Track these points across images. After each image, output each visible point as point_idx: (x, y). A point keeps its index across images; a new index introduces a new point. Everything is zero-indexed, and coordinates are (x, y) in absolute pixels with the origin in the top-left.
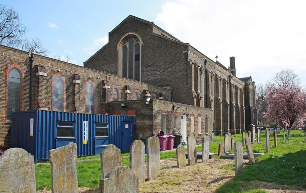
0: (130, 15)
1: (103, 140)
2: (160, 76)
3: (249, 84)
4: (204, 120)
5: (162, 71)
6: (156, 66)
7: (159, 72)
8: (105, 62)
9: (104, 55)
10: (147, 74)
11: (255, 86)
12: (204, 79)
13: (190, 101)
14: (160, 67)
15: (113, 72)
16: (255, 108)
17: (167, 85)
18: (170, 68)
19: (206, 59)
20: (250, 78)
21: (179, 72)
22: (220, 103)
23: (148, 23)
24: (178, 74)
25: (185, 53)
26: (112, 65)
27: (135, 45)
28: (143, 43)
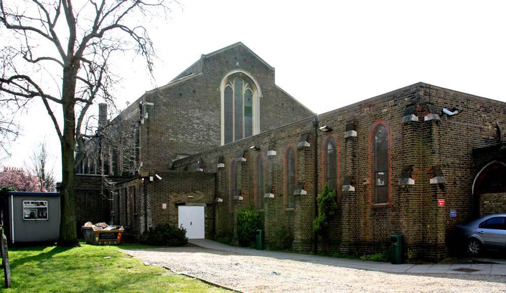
1: (38, 92)
8: (196, 103)
15: (212, 124)
26: (210, 112)
27: (246, 91)
28: (262, 94)
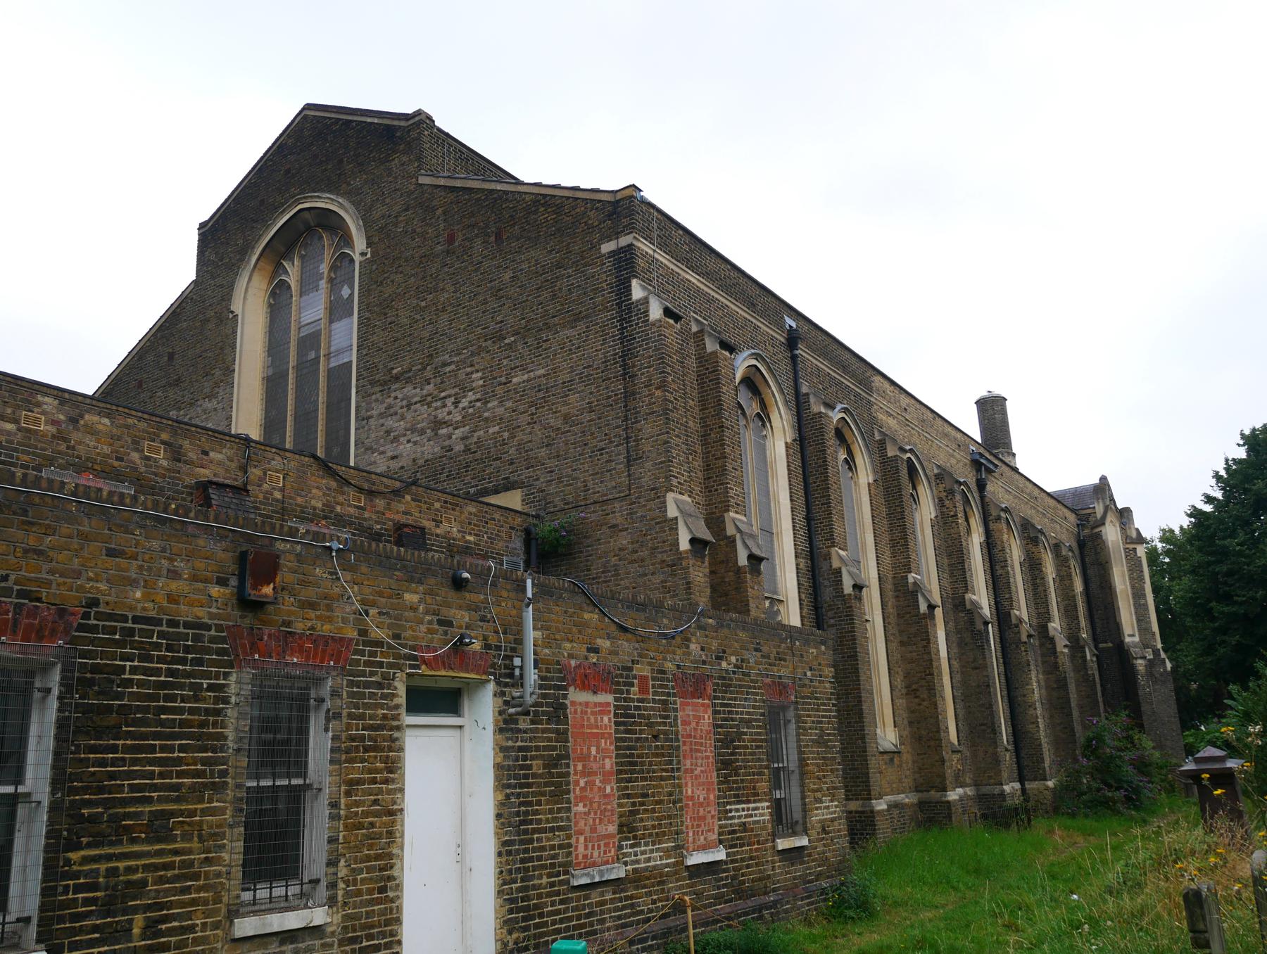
0: (309, 107)
2: (458, 433)
3: (1099, 516)
4: (748, 723)
5: (471, 396)
6: (436, 373)
7: (456, 403)
9: (171, 356)
10: (388, 432)
11: (1134, 535)
12: (787, 446)
13: (658, 579)
14: (461, 375)
16: (1156, 652)
17: (508, 486)
18: (524, 368)
19: (790, 322)
20: (1102, 489)
21: (581, 387)
22: (923, 608)
23: (396, 123)
24: (573, 398)
25: (613, 254)
28: (369, 245)
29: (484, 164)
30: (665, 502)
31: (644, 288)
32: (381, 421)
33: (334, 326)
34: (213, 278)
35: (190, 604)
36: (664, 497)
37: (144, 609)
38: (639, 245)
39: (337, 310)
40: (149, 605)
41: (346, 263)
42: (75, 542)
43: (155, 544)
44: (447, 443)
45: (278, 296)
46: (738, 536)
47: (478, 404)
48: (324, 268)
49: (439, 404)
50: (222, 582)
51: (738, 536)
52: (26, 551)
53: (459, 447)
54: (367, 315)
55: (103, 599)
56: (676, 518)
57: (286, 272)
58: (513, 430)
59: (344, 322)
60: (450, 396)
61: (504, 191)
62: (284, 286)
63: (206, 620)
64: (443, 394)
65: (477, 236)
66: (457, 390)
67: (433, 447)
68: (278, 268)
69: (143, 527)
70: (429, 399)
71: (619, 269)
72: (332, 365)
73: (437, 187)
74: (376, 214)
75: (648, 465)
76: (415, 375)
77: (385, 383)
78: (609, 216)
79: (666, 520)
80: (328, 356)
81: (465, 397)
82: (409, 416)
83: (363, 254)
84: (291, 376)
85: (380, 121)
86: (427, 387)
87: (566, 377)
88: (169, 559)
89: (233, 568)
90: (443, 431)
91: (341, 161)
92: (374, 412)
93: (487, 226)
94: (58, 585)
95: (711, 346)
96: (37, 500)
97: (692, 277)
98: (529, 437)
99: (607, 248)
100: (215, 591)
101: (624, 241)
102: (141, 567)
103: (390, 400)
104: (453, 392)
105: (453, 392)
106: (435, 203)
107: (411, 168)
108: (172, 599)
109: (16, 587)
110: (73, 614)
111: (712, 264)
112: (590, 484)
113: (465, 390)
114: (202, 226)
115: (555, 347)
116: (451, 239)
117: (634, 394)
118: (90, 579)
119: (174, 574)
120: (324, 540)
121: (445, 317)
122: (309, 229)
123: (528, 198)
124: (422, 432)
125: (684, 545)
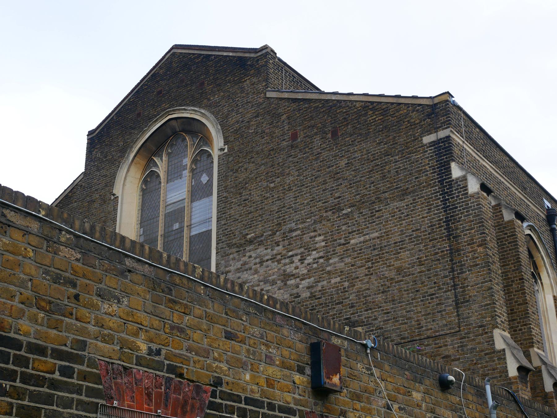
0: (176, 47)
2: (305, 283)
5: (315, 254)
6: (284, 237)
7: (302, 260)
18: (360, 232)
23: (247, 55)
24: (404, 255)
25: (433, 144)
28: (226, 143)
29: (308, 86)
30: (492, 337)
31: (462, 169)
32: (238, 275)
33: (195, 204)
34: (98, 170)
35: (281, 390)
36: (492, 332)
37: (252, 391)
38: (454, 137)
39: (199, 192)
40: (255, 387)
41: (204, 157)
42: (204, 324)
43: (256, 330)
44: (295, 291)
45: (150, 182)
46: (543, 367)
47: (321, 261)
48: (187, 161)
49: (287, 261)
50: (301, 371)
51: (543, 367)
52: (172, 328)
53: (306, 294)
54: (225, 194)
55: (226, 379)
56: (504, 350)
57: (156, 165)
58: (353, 280)
59: (205, 200)
60: (296, 255)
61: (338, 101)
62: (154, 175)
63: (292, 405)
64: (290, 253)
65: (316, 134)
66: (302, 250)
67: (283, 294)
68: (150, 162)
69: (248, 314)
70: (279, 257)
71: (439, 155)
72: (193, 233)
73: (281, 99)
74: (231, 121)
75: (475, 307)
76: (266, 239)
77: (241, 245)
78: (429, 116)
79: (494, 351)
80: (190, 227)
81: (309, 255)
82: (262, 271)
83: (222, 149)
84: (159, 242)
85: (234, 54)
86: (277, 248)
87: (398, 239)
88: (266, 345)
89: (307, 358)
90: (292, 282)
91: (202, 84)
92: (232, 268)
93: (324, 126)
94: (194, 362)
95: (508, 216)
96: (177, 281)
97: (486, 164)
98: (367, 286)
99: (427, 139)
100: (297, 378)
101: (442, 134)
102: (248, 351)
103: (246, 259)
104: (299, 251)
105: (299, 251)
106: (280, 111)
107: (260, 87)
108: (270, 383)
109: (167, 362)
110: (206, 392)
111: (499, 156)
112: (423, 323)
113: (309, 250)
114: (90, 133)
115: (386, 215)
116: (294, 137)
117: (458, 250)
118: (215, 359)
119: (269, 360)
120: (360, 339)
121: (291, 194)
122: (175, 134)
123: (358, 105)
124: (273, 283)
125: (513, 372)
